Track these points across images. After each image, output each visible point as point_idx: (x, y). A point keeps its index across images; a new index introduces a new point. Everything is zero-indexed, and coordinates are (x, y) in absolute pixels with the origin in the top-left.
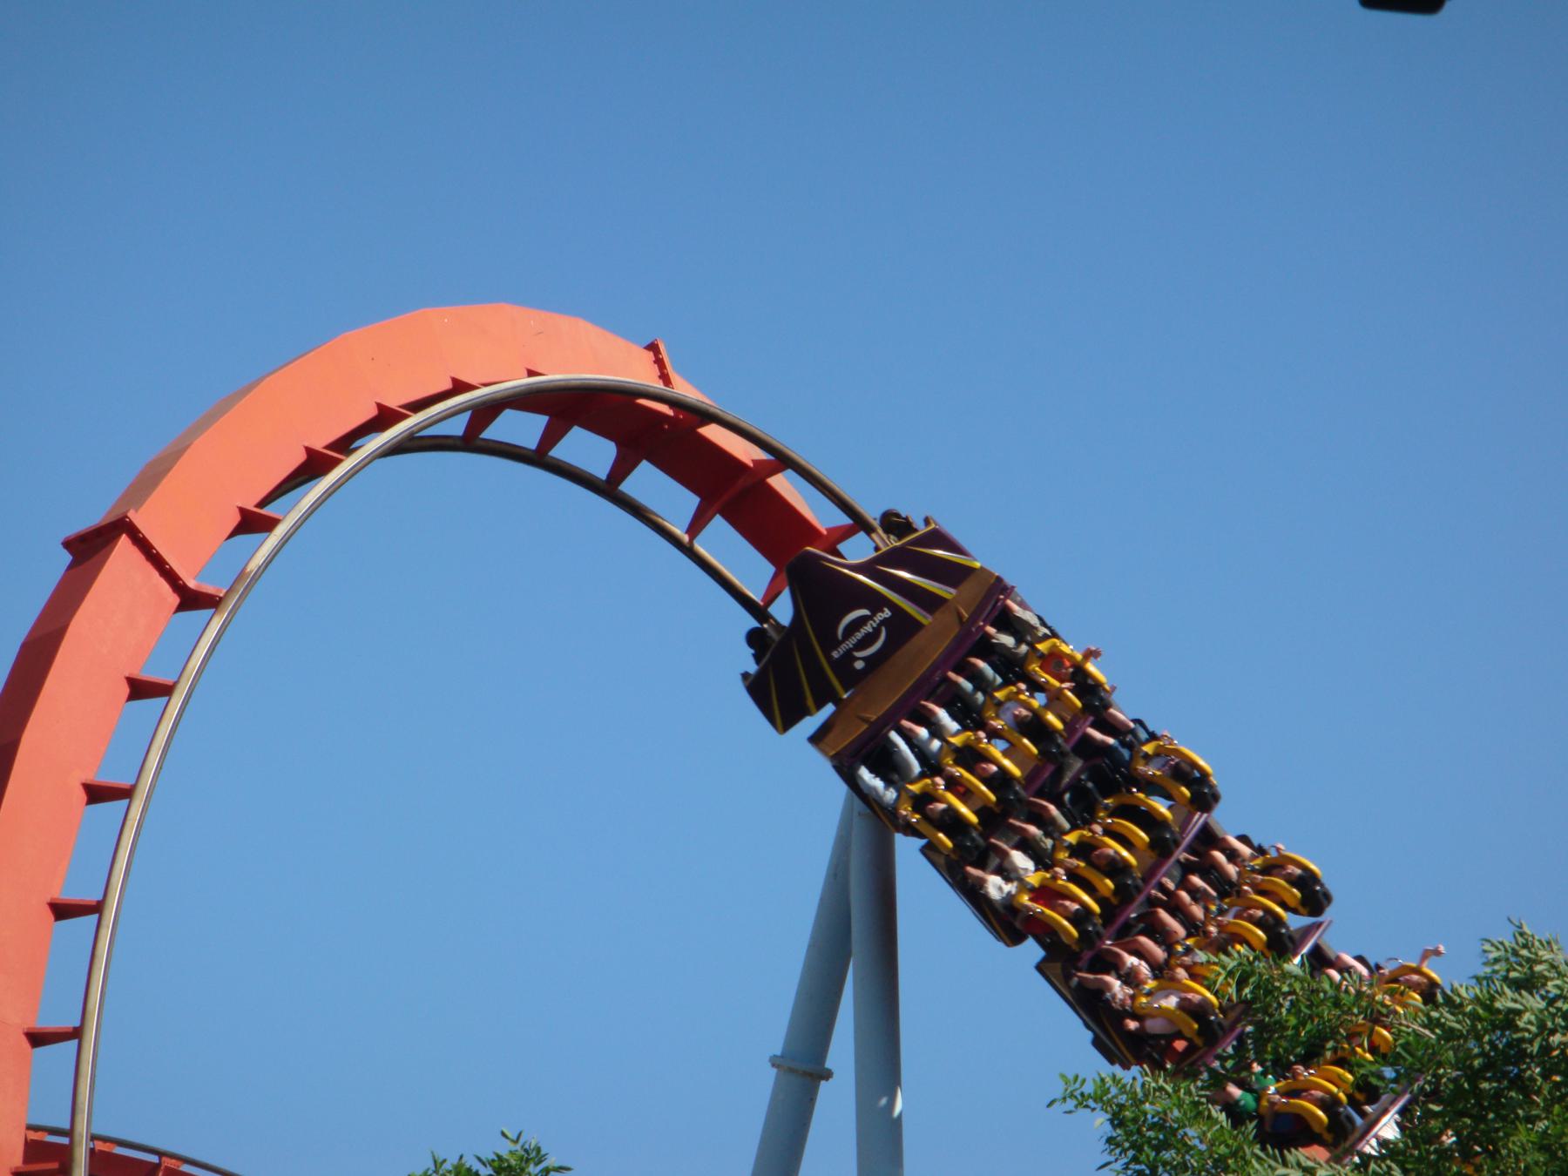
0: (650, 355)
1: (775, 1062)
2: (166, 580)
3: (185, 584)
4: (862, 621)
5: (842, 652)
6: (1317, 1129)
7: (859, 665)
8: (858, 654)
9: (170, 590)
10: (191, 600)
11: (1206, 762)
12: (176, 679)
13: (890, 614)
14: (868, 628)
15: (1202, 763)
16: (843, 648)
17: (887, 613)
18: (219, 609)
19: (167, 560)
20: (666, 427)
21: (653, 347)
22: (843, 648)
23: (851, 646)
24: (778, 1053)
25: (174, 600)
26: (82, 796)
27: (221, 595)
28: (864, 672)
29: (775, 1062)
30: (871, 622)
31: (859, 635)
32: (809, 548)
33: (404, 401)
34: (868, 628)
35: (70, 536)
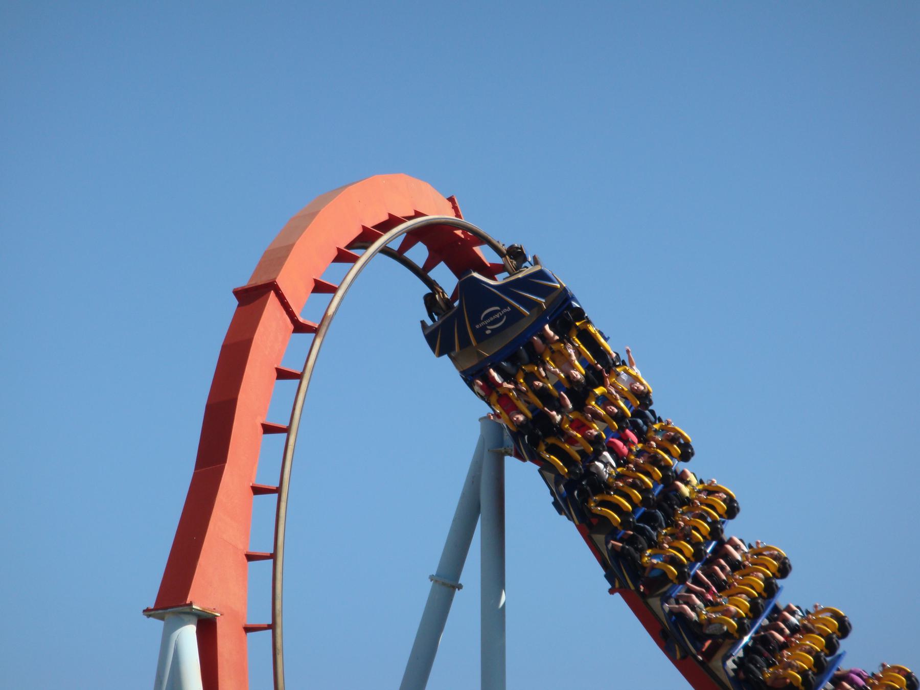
0: (450, 204)
1: (432, 578)
2: (289, 317)
3: (297, 320)
4: (495, 312)
5: (481, 326)
6: (671, 577)
7: (488, 332)
8: (488, 327)
9: (290, 322)
10: (300, 328)
11: (688, 435)
12: (302, 371)
13: (510, 310)
14: (498, 316)
15: (686, 435)
16: (483, 323)
17: (509, 309)
18: (318, 333)
19: (291, 305)
20: (460, 243)
21: (451, 199)
22: (483, 323)
23: (486, 323)
24: (434, 573)
25: (291, 327)
26: (260, 429)
27: (317, 327)
28: (489, 335)
29: (432, 578)
30: (500, 313)
31: (492, 319)
32: (476, 275)
33: (372, 226)
34: (498, 316)
35: (237, 288)
